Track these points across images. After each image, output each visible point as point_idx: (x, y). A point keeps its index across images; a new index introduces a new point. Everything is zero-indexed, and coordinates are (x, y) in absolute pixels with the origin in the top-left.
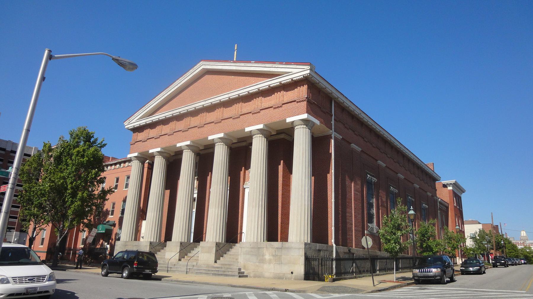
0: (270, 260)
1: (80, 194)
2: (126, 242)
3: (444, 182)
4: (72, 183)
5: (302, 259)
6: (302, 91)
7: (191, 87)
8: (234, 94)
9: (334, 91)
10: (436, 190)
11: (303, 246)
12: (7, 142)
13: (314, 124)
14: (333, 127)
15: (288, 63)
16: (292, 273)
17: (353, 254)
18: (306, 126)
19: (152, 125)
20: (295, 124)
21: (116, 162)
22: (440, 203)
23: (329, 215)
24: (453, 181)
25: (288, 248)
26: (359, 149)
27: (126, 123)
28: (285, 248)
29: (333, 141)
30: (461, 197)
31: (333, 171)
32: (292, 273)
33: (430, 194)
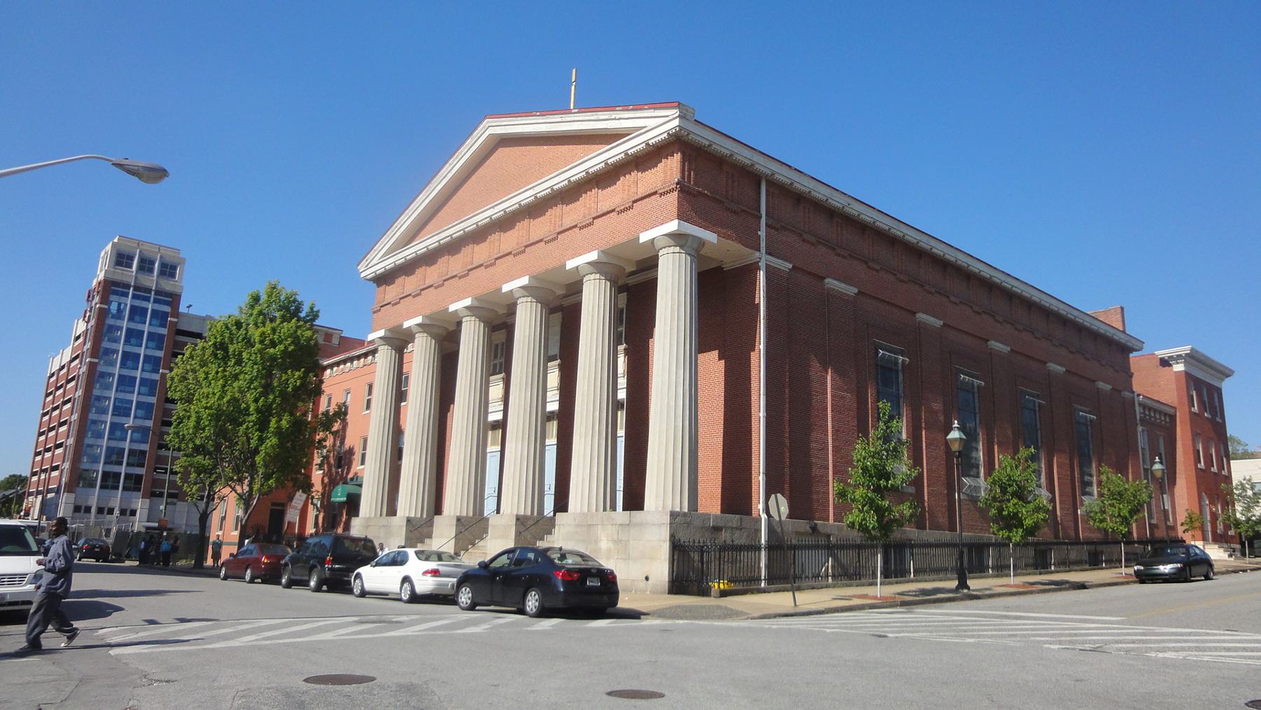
0: (609, 550)
1: (273, 423)
2: (369, 518)
3: (1162, 353)
4: (256, 401)
5: (666, 548)
6: (671, 167)
7: (474, 177)
8: (542, 188)
9: (757, 159)
10: (1131, 376)
11: (667, 519)
12: (204, 319)
13: (702, 243)
14: (763, 244)
15: (638, 107)
16: (647, 578)
17: (828, 536)
18: (681, 247)
19: (406, 269)
20: (658, 244)
21: (364, 351)
22: (1140, 404)
23: (754, 449)
24: (1185, 350)
25: (641, 525)
26: (852, 290)
27: (361, 268)
28: (636, 525)
29: (762, 276)
30: (1219, 391)
31: (762, 347)
32: (647, 578)
33: (1104, 386)
